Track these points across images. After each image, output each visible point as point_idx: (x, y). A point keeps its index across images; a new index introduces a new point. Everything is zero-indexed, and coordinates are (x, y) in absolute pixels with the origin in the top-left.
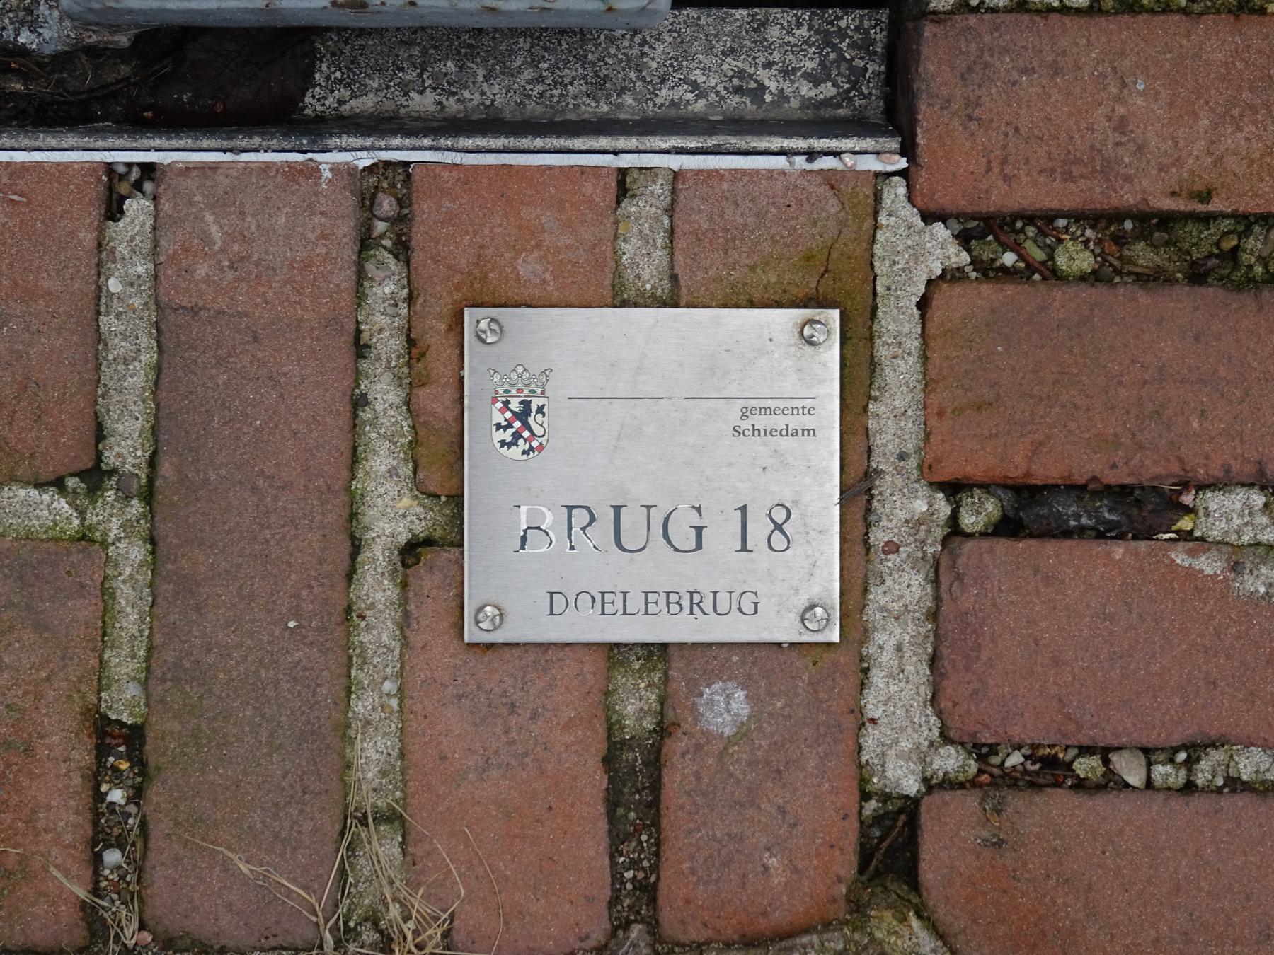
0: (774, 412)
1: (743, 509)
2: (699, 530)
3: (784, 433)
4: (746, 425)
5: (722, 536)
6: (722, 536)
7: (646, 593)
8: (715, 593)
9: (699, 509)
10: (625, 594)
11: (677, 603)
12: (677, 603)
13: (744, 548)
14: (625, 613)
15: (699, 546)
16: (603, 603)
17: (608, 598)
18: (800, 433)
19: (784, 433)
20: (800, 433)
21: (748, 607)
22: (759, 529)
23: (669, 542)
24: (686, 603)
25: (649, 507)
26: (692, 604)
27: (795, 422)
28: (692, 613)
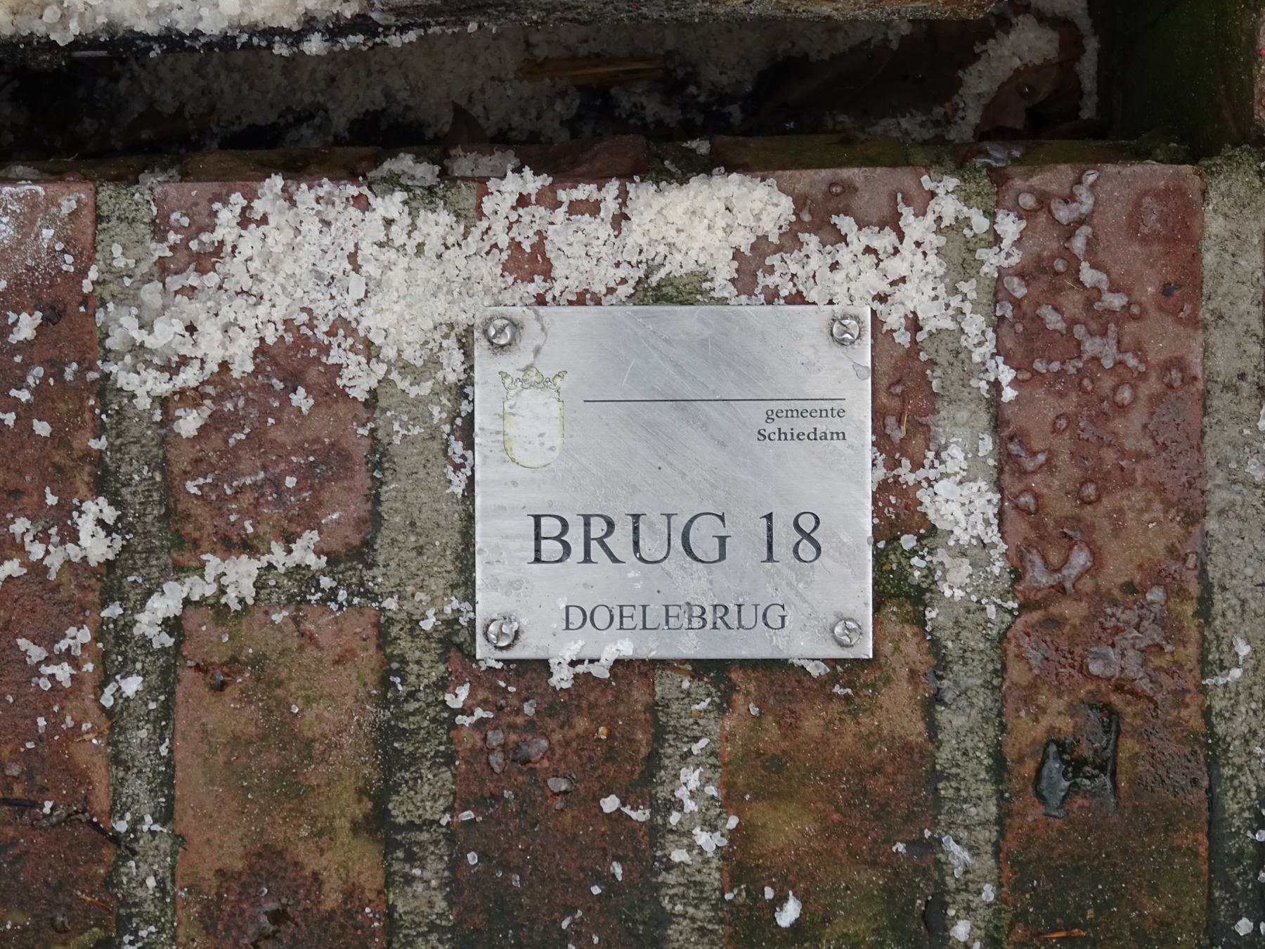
0: (801, 414)
1: (769, 517)
2: (722, 540)
3: (812, 436)
4: (771, 428)
5: (745, 551)
6: (745, 551)
7: (667, 607)
8: (636, 517)
9: (722, 518)
10: (644, 607)
11: (557, 538)
12: (557, 538)
13: (770, 558)
14: (644, 627)
15: (722, 556)
16: (622, 616)
17: (627, 612)
18: (829, 437)
19: (812, 436)
20: (829, 437)
21: (704, 543)
22: (785, 536)
23: (696, 559)
24: (575, 537)
25: (669, 516)
26: (587, 539)
27: (823, 425)
28: (587, 559)
